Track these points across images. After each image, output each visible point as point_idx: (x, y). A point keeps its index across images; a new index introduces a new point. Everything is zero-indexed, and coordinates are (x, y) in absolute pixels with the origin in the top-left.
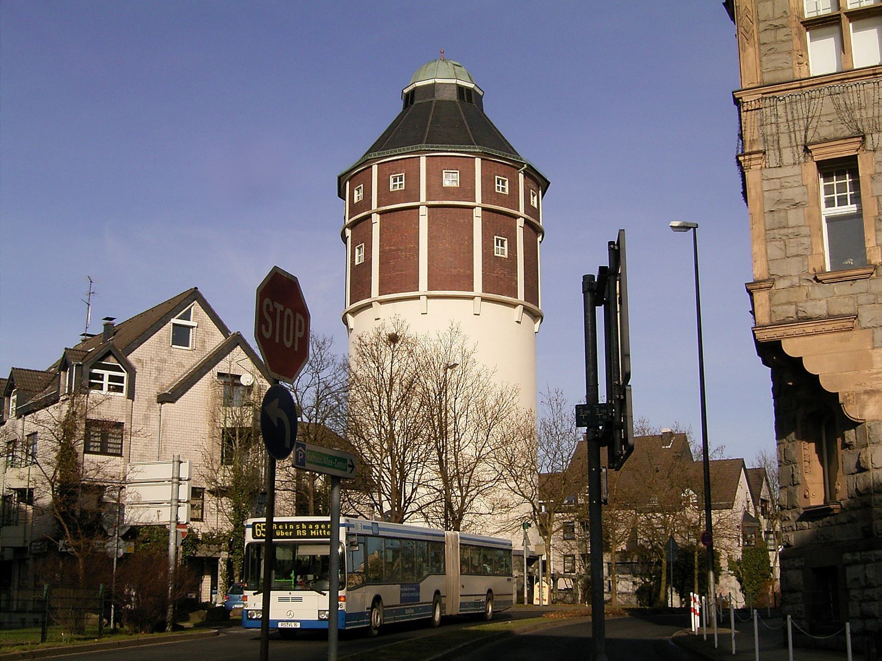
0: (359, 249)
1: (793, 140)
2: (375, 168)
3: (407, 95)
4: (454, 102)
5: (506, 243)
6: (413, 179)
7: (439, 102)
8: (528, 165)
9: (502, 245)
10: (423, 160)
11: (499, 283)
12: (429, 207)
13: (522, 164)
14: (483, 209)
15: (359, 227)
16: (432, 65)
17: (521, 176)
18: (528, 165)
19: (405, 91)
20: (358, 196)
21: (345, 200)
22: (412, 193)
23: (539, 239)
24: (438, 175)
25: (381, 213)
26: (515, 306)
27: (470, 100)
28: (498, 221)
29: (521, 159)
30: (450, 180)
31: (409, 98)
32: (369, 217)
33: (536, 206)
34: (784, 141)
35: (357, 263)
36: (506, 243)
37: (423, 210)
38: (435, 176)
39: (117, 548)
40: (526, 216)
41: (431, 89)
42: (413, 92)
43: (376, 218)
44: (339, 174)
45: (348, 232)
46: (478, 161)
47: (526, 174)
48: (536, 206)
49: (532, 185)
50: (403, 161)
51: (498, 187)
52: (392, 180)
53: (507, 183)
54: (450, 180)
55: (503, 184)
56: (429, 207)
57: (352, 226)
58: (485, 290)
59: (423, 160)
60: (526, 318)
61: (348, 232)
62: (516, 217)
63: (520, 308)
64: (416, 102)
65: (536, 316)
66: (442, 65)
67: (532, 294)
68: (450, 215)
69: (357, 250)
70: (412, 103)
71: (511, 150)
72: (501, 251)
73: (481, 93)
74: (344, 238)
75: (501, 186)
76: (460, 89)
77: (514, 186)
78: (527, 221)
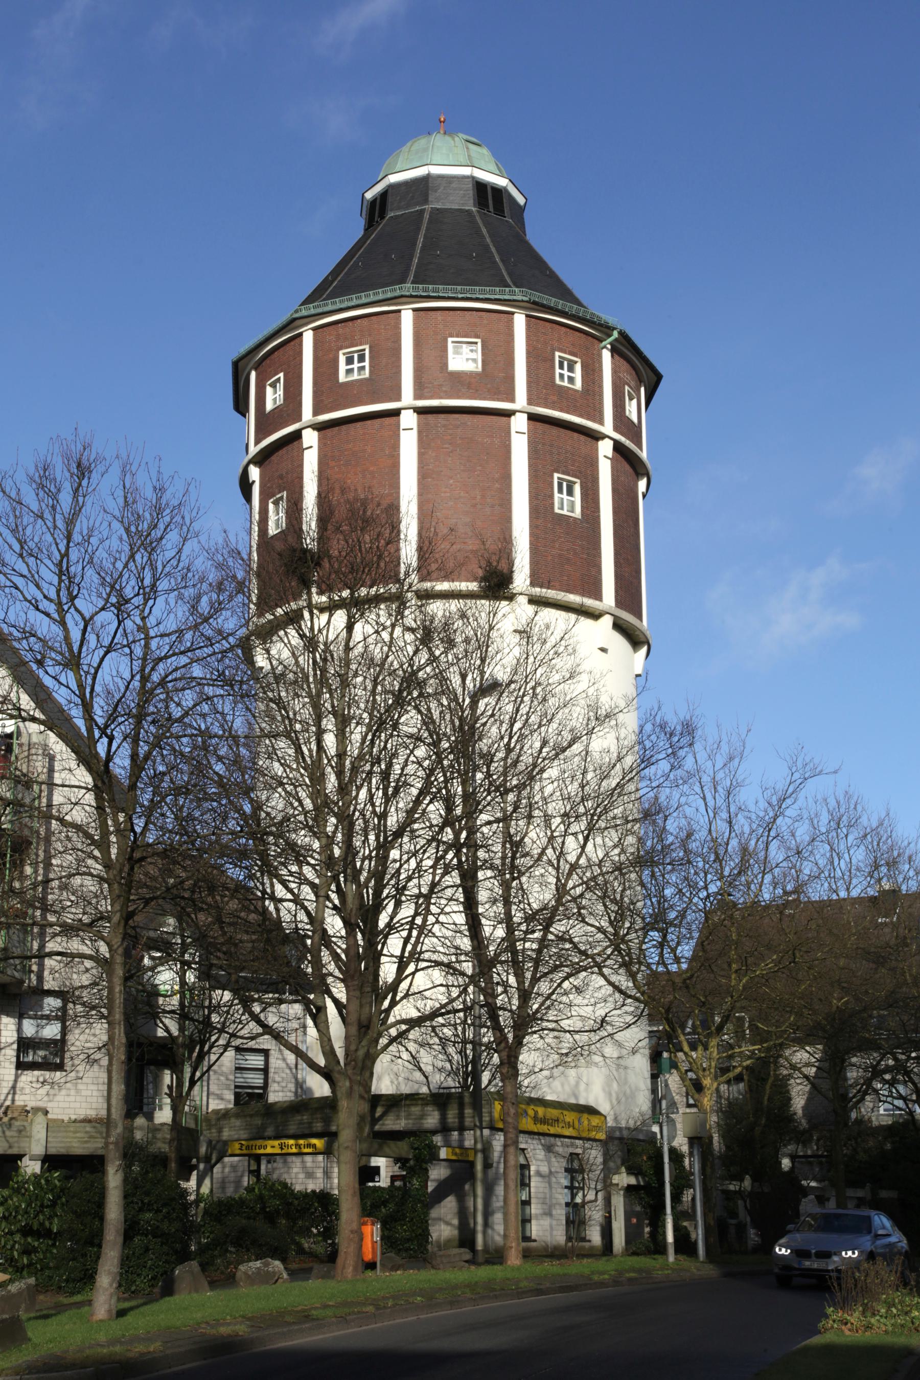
0: (276, 503)
2: (308, 338)
3: (373, 202)
4: (469, 212)
5: (577, 489)
7: (437, 213)
9: (570, 493)
10: (407, 318)
12: (420, 411)
14: (532, 417)
16: (422, 142)
17: (606, 355)
18: (622, 334)
19: (369, 195)
20: (273, 398)
22: (384, 382)
23: (642, 485)
25: (320, 427)
26: (595, 615)
27: (499, 209)
28: (562, 442)
30: (464, 358)
31: (377, 210)
32: (296, 436)
33: (635, 419)
35: (272, 530)
36: (577, 489)
37: (408, 420)
40: (617, 436)
41: (423, 185)
42: (384, 195)
43: (310, 438)
44: (235, 356)
45: (255, 473)
46: (520, 321)
47: (614, 351)
48: (635, 420)
49: (627, 375)
50: (365, 322)
51: (562, 376)
52: (342, 359)
53: (578, 367)
54: (464, 358)
55: (571, 369)
56: (420, 411)
57: (261, 459)
59: (407, 318)
60: (619, 642)
62: (596, 437)
63: (607, 620)
64: (391, 214)
65: (635, 639)
69: (271, 507)
70: (382, 216)
72: (568, 504)
73: (521, 200)
74: (246, 486)
75: (566, 372)
76: (481, 187)
77: (592, 373)
78: (618, 447)
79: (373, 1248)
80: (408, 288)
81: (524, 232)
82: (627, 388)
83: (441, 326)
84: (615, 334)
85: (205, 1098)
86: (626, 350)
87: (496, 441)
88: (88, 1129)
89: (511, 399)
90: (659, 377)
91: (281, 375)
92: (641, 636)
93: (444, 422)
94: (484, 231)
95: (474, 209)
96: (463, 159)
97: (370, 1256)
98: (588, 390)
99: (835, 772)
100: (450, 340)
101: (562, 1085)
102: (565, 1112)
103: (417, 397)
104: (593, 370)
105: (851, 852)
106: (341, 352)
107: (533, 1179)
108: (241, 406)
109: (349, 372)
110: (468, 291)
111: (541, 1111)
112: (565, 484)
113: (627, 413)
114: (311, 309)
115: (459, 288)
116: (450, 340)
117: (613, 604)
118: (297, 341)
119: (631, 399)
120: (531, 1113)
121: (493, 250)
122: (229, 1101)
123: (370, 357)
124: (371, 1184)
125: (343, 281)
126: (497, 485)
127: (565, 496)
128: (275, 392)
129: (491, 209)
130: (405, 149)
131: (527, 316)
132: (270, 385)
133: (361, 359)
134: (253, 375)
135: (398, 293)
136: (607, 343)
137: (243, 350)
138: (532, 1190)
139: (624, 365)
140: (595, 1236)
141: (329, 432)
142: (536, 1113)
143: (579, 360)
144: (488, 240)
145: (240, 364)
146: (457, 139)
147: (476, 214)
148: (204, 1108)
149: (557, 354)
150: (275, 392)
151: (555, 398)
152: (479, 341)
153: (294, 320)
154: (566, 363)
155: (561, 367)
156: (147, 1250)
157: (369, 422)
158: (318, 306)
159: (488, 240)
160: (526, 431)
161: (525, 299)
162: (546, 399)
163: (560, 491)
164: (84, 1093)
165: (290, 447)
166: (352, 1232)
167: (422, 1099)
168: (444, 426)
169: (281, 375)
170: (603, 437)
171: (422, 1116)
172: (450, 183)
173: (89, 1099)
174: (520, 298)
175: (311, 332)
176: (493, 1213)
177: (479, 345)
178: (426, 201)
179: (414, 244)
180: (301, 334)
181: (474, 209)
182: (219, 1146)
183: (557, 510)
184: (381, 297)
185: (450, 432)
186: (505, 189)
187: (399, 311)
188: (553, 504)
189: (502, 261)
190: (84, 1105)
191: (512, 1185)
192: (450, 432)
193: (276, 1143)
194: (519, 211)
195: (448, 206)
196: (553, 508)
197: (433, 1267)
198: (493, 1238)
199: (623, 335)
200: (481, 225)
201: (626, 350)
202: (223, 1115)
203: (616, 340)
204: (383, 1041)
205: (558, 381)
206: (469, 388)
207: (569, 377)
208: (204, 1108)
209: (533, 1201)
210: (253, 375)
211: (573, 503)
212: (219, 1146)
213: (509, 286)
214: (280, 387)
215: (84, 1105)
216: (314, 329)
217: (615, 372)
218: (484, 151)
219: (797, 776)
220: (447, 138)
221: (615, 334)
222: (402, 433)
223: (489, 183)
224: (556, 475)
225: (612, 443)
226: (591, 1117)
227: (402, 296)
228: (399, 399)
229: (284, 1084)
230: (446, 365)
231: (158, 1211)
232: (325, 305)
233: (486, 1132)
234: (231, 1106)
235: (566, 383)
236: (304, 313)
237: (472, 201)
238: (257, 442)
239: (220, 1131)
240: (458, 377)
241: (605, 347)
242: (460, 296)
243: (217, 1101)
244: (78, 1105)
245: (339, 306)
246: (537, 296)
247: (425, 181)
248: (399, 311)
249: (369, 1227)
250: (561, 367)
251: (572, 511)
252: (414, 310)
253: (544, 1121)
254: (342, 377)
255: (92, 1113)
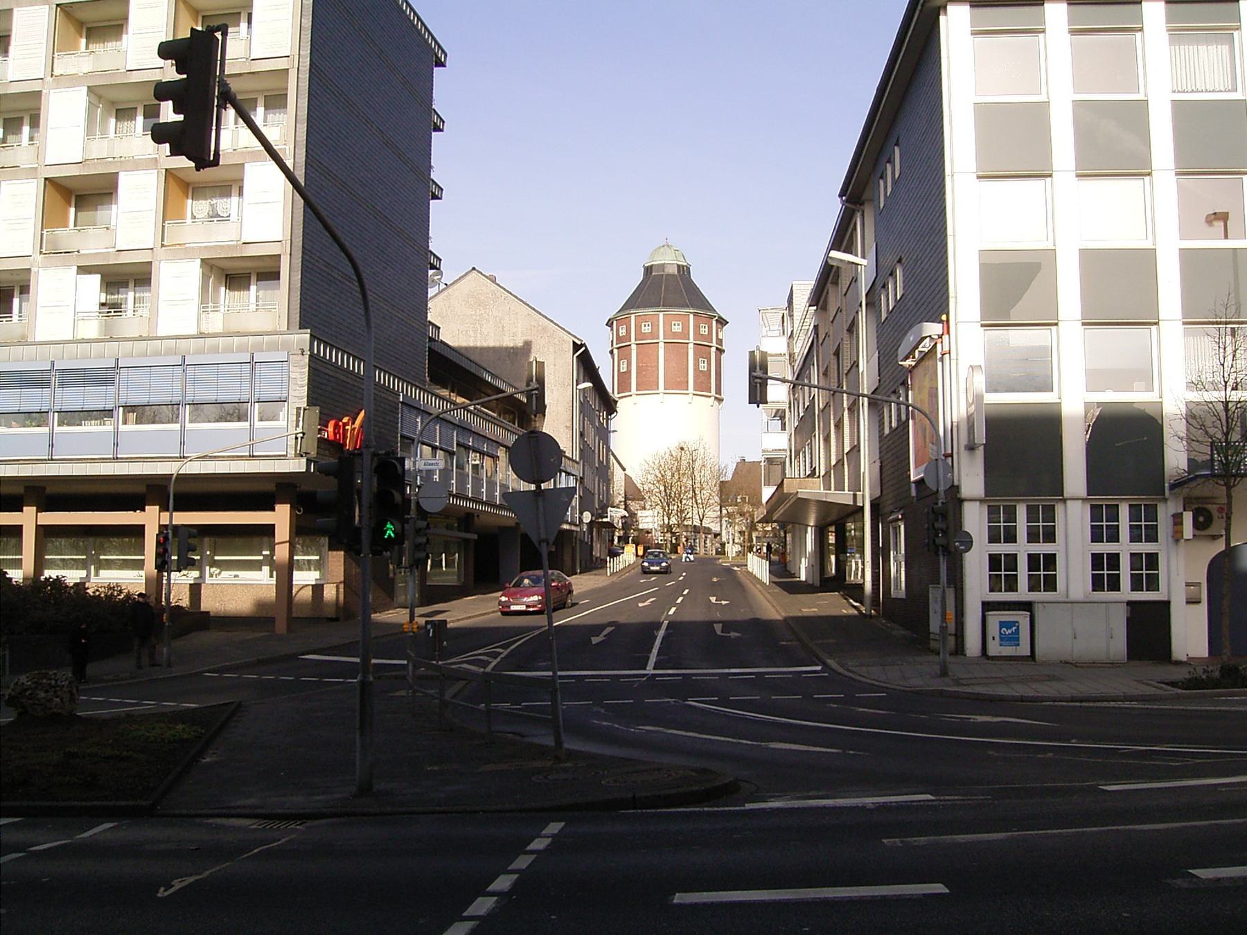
1: (541, 509)
6: (655, 326)
11: (702, 385)
22: (654, 334)
24: (664, 322)
28: (702, 349)
34: (406, 391)
38: (668, 325)
39: (398, 497)
41: (663, 266)
45: (616, 351)
54: (677, 328)
67: (718, 391)
68: (676, 346)
71: (709, 307)
72: (703, 366)
76: (679, 266)
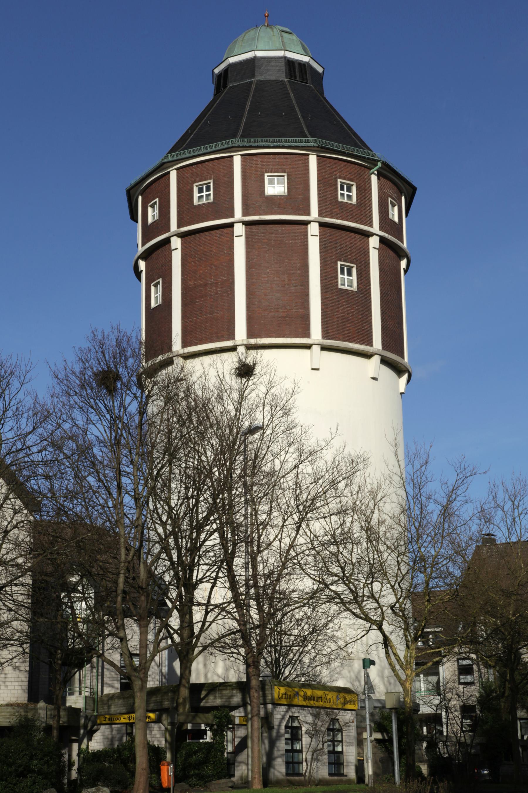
0: (156, 286)
2: (173, 175)
3: (219, 75)
4: (282, 82)
5: (354, 271)
8: (384, 163)
9: (350, 274)
10: (237, 161)
11: (346, 327)
12: (246, 224)
13: (374, 162)
14: (322, 225)
15: (157, 255)
16: (252, 33)
17: (374, 179)
18: (384, 163)
19: (217, 71)
20: (152, 215)
21: (137, 222)
23: (403, 264)
26: (368, 356)
27: (303, 78)
28: (343, 243)
29: (374, 155)
31: (222, 80)
32: (167, 241)
33: (396, 219)
35: (153, 305)
36: (354, 271)
37: (239, 230)
41: (251, 64)
42: (226, 71)
43: (176, 243)
44: (128, 186)
45: (142, 265)
46: (313, 159)
48: (396, 219)
49: (390, 190)
50: (210, 164)
51: (342, 195)
52: (196, 190)
53: (354, 188)
54: (276, 187)
56: (246, 224)
57: (145, 256)
58: (326, 334)
59: (237, 161)
60: (387, 372)
61: (142, 265)
62: (368, 235)
63: (376, 359)
65: (398, 370)
66: (263, 32)
67: (393, 339)
70: (225, 87)
71: (361, 144)
72: (348, 281)
73: (320, 70)
74: (138, 273)
75: (345, 193)
76: (290, 64)
78: (383, 240)
79: (169, 779)
80: (237, 141)
81: (322, 93)
82: (390, 199)
83: (260, 166)
84: (379, 164)
85: (100, 687)
86: (388, 174)
87: (298, 242)
88: (8, 710)
89: (308, 214)
90: (414, 189)
91: (157, 200)
92: (402, 367)
93: (263, 230)
94: (292, 95)
95: (285, 80)
96: (279, 45)
97: (166, 785)
98: (361, 204)
99: (485, 473)
100: (266, 175)
101: (349, 672)
102: (327, 692)
103: (245, 214)
104: (365, 190)
105: (521, 518)
106: (195, 185)
107: (304, 736)
108: (134, 217)
109: (200, 198)
110: (277, 142)
111: (309, 692)
112: (346, 268)
113: (390, 216)
114: (175, 156)
115: (271, 139)
116: (266, 175)
117: (380, 348)
118: (166, 177)
119: (393, 206)
120: (302, 693)
121: (297, 109)
122: (117, 689)
123: (214, 188)
124: (201, 741)
125: (199, 135)
126: (299, 272)
127: (346, 277)
128: (154, 211)
129: (298, 79)
130: (240, 38)
131: (318, 156)
132: (151, 206)
133: (208, 189)
134: (140, 198)
135: (231, 145)
136: (375, 170)
137: (133, 181)
138: (304, 743)
139: (388, 183)
140: (351, 772)
141: (188, 239)
142: (305, 693)
143: (354, 183)
144: (294, 102)
145: (131, 191)
146: (275, 30)
147: (287, 84)
148: (100, 693)
149: (339, 180)
150: (154, 211)
151: (338, 211)
152: (285, 174)
153: (164, 163)
154: (345, 186)
155: (342, 189)
156: (34, 783)
157: (214, 232)
158: (179, 154)
159: (294, 102)
160: (318, 234)
161: (316, 145)
162: (331, 212)
163: (342, 273)
164: (9, 687)
165: (163, 249)
166: (142, 769)
167: (230, 686)
168: (263, 233)
169: (157, 200)
170: (372, 234)
171: (232, 696)
172: (270, 62)
173: (13, 691)
174: (311, 144)
175: (175, 171)
176: (274, 759)
177: (286, 178)
178: (253, 76)
179: (244, 108)
180: (169, 173)
181: (285, 80)
182: (92, 718)
183: (340, 287)
184: (220, 147)
185: (267, 237)
186: (308, 63)
187: (232, 156)
188: (337, 282)
189: (303, 117)
190: (9, 695)
191: (256, 740)
192: (267, 237)
193: (126, 716)
194: (318, 78)
195: (268, 78)
196: (337, 285)
197: (210, 791)
198: (274, 774)
199: (385, 165)
200: (290, 91)
201: (388, 174)
202: (111, 697)
203: (380, 168)
204: (197, 650)
205: (340, 199)
206: (279, 207)
207: (347, 195)
208: (100, 693)
209: (304, 750)
210: (140, 198)
211: (351, 281)
212: (92, 718)
213: (306, 136)
214: (157, 207)
215: (9, 695)
216: (177, 169)
217: (380, 189)
218: (294, 37)
219: (461, 476)
220: (269, 30)
221: (379, 164)
222: (235, 239)
223: (296, 60)
224: (339, 263)
225: (378, 238)
226: (346, 695)
227: (233, 147)
228: (232, 216)
229: (153, 676)
230: (264, 191)
231: (41, 759)
232: (184, 153)
233: (270, 706)
234: (119, 691)
235: (346, 200)
236: (170, 159)
237: (284, 74)
238: (143, 245)
239: (109, 707)
240: (273, 199)
241: (373, 173)
242: (272, 145)
243: (110, 689)
244: (6, 695)
245: (193, 154)
246: (324, 143)
247: (253, 61)
248: (232, 156)
249: (166, 767)
250: (342, 189)
251: (351, 286)
252: (242, 155)
253: (311, 698)
254: (196, 202)
255: (13, 700)
